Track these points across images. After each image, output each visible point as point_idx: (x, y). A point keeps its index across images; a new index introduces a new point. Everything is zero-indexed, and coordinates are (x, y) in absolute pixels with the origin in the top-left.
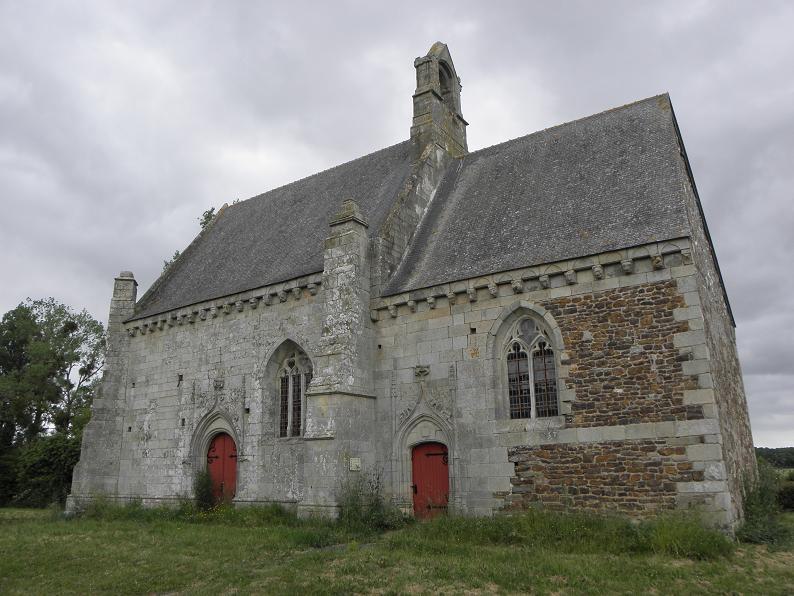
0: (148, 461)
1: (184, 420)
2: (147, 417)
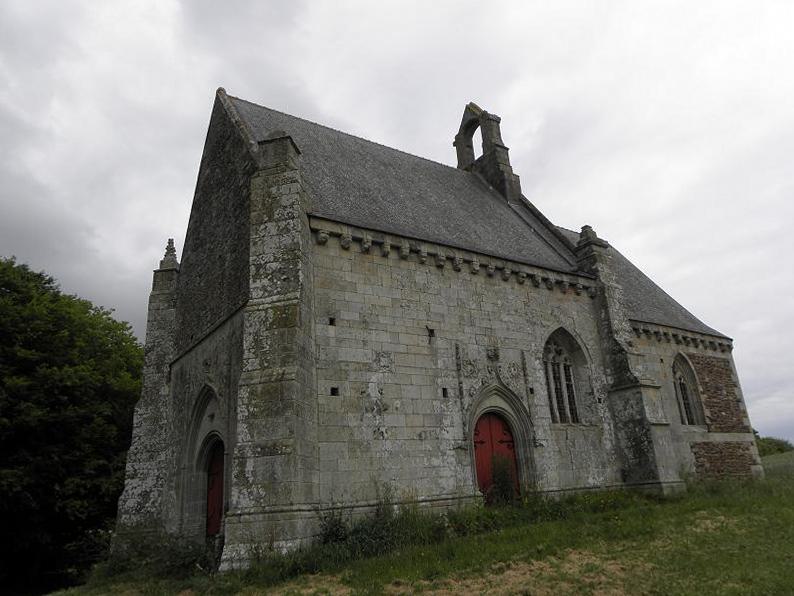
0: (388, 445)
1: (445, 390)
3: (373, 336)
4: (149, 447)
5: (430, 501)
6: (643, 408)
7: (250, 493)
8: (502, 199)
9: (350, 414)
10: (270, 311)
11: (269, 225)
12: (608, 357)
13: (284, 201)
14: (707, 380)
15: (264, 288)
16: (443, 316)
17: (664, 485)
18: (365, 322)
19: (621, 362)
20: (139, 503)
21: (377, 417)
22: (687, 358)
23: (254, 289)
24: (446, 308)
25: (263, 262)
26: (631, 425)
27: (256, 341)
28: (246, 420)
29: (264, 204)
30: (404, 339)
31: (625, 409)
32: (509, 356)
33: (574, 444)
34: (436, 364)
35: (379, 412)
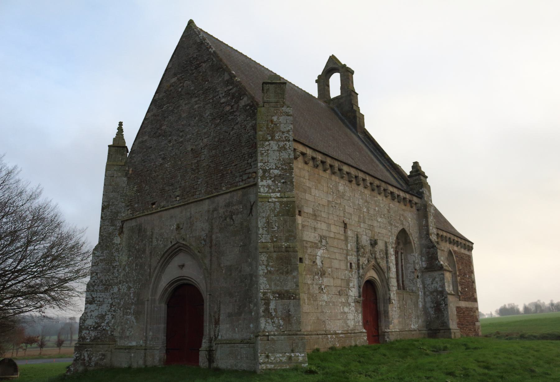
0: (325, 297)
1: (351, 264)
2: (320, 252)
3: (319, 225)
4: (104, 282)
5: (344, 334)
6: (444, 284)
7: (273, 322)
8: (354, 130)
9: (308, 276)
10: (277, 203)
11: (272, 142)
12: (424, 249)
13: (283, 127)
14: (461, 268)
15: (269, 186)
16: (351, 214)
17: (452, 331)
18: (315, 215)
19: (433, 254)
20: (96, 323)
21: (321, 279)
22: (453, 252)
23: (261, 186)
24: (353, 210)
25: (267, 168)
26: (435, 294)
27: (268, 223)
28: (265, 275)
29: (267, 128)
30: (333, 228)
31: (432, 284)
32: (381, 245)
33: (406, 303)
34: (347, 247)
35: (321, 276)
